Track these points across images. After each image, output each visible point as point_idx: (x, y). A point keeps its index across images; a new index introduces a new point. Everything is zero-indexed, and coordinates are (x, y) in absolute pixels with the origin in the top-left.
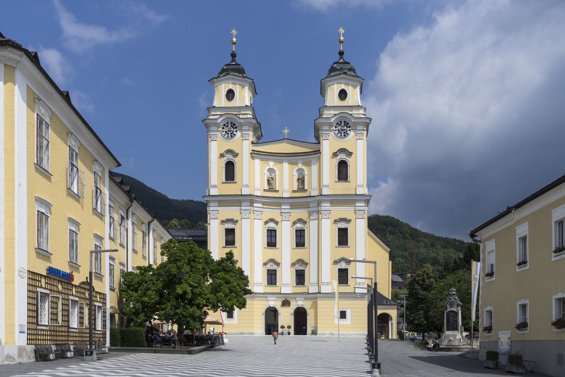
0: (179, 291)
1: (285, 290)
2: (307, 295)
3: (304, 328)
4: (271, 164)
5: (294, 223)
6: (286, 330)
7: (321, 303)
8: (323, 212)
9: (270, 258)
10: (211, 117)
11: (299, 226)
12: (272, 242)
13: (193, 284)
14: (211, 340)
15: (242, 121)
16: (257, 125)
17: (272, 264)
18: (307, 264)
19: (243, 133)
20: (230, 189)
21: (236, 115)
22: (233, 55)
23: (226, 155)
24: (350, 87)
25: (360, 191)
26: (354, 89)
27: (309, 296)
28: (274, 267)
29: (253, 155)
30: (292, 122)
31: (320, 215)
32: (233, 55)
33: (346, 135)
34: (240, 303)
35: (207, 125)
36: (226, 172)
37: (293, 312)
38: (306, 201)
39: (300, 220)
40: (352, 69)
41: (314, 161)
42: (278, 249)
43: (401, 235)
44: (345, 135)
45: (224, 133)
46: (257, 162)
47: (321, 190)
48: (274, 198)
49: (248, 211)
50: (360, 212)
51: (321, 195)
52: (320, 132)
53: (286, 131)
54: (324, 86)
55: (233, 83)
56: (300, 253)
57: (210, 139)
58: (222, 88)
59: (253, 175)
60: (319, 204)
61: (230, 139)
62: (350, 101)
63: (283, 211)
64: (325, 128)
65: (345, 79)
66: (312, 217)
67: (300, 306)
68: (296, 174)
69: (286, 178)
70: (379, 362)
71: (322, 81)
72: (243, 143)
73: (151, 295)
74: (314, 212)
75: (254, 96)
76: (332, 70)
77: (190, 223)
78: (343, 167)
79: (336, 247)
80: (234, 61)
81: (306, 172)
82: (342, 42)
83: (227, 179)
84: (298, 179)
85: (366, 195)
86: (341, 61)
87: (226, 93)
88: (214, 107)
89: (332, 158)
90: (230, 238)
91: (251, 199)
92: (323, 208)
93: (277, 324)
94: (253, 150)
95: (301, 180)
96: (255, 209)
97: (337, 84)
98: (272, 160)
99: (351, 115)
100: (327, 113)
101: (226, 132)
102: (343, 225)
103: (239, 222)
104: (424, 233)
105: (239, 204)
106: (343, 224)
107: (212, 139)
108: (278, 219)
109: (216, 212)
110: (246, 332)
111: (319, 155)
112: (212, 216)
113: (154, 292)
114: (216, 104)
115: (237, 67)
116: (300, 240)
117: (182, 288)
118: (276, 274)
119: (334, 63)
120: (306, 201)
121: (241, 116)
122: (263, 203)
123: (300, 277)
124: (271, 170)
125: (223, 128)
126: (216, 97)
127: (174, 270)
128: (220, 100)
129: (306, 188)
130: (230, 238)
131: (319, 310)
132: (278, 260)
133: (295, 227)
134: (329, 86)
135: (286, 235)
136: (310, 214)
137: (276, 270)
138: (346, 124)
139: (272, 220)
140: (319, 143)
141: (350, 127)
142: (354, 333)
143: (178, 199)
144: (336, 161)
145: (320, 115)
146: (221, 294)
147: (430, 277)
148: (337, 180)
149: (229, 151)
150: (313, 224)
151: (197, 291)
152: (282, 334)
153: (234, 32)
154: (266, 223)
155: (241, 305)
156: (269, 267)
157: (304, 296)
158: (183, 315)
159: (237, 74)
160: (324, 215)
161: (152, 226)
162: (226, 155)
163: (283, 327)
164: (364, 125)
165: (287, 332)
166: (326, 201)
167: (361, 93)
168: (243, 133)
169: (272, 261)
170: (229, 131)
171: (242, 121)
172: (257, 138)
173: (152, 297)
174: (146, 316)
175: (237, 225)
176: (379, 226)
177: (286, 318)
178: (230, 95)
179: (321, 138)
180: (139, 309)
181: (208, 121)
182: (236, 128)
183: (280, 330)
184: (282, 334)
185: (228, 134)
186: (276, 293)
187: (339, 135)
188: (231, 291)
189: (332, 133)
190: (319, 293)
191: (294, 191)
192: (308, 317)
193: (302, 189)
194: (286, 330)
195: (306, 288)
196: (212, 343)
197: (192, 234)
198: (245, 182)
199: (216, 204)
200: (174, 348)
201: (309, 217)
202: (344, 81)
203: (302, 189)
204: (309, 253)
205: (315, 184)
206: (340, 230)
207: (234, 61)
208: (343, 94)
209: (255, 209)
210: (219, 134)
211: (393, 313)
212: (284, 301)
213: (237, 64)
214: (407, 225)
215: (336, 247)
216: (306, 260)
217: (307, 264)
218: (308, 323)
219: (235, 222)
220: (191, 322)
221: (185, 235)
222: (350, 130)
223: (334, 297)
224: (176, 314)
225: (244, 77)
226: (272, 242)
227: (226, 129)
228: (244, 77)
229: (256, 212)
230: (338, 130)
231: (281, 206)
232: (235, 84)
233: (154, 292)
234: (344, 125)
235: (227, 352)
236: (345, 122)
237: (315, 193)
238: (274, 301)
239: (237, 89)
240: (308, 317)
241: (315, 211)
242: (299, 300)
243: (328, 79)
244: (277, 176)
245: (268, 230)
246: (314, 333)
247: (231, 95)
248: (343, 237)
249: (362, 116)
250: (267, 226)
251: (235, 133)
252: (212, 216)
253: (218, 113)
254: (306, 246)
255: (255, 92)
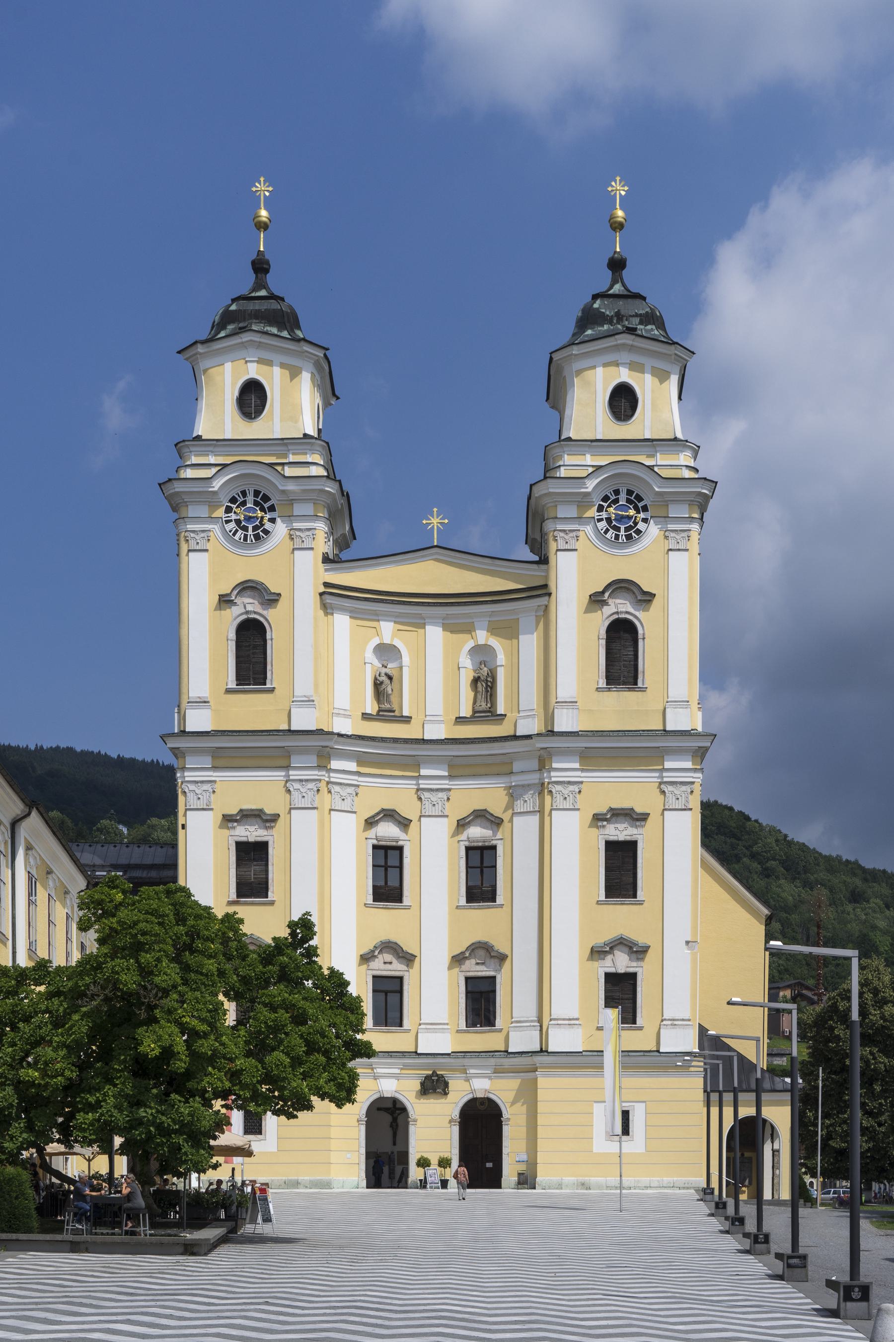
0: (150, 1047)
1: (430, 1043)
2: (502, 1059)
3: (489, 1165)
4: (388, 631)
5: (462, 825)
6: (434, 1173)
7: (549, 1086)
8: (555, 789)
9: (384, 937)
10: (189, 473)
11: (477, 833)
12: (388, 889)
13: (194, 1022)
14: (227, 1209)
15: (291, 487)
16: (341, 501)
17: (388, 957)
18: (502, 958)
19: (296, 525)
20: (252, 712)
21: (271, 465)
22: (260, 267)
23: (239, 600)
24: (648, 377)
25: (678, 720)
26: (662, 381)
27: (508, 1062)
28: (396, 968)
29: (329, 600)
30: (456, 490)
31: (548, 798)
32: (260, 267)
33: (633, 534)
34: (340, 1086)
35: (176, 501)
36: (238, 657)
37: (456, 1114)
38: (499, 751)
39: (481, 816)
40: (653, 318)
41: (526, 621)
42: (408, 908)
43: (755, 865)
44: (629, 537)
45: (232, 525)
46: (342, 622)
47: (549, 718)
48: (396, 740)
49: (310, 785)
50: (678, 790)
51: (551, 733)
52: (549, 526)
53: (435, 521)
54: (560, 370)
55: (260, 361)
56: (482, 923)
57: (184, 547)
58: (226, 377)
59: (328, 667)
60: (543, 763)
61: (252, 546)
62: (647, 423)
63: (424, 784)
64: (563, 511)
65: (631, 349)
66: (519, 806)
67: (480, 1095)
68: (467, 662)
69: (436, 675)
70: (863, 1279)
71: (556, 357)
72: (295, 559)
73: (53, 1061)
74: (526, 787)
75: (327, 404)
76: (588, 318)
77: (69, 823)
78: (622, 639)
79: (598, 903)
80: (264, 286)
81: (501, 658)
82: (621, 226)
83: (241, 678)
84: (476, 681)
85: (699, 735)
86: (617, 288)
87: (236, 393)
88: (199, 438)
89: (587, 611)
90: (252, 872)
91: (321, 745)
92: (556, 776)
93: (404, 1157)
94: (326, 585)
95: (485, 684)
96: (335, 777)
97: (605, 365)
98: (387, 617)
99: (651, 468)
100: (573, 464)
101: (238, 522)
102: (620, 832)
103: (281, 822)
104: (828, 859)
105: (283, 763)
106: (621, 826)
107: (193, 546)
108: (408, 808)
109: (207, 787)
110: (304, 1178)
111: (543, 601)
112: (193, 802)
113: (62, 1053)
114: (204, 428)
115: (274, 305)
116: (481, 879)
117: (160, 1038)
118: (401, 992)
119: (595, 297)
120: (499, 751)
121: (288, 471)
122: (362, 759)
123: (481, 1004)
124: (386, 651)
125: (228, 510)
126: (204, 404)
127: (130, 980)
128: (217, 416)
129: (500, 710)
130: (252, 872)
131: (541, 1107)
132: (409, 946)
133: (463, 837)
134: (579, 372)
135: (435, 865)
136: (513, 794)
137: (401, 979)
138: (635, 500)
139: (389, 815)
140: (544, 561)
141: (645, 509)
142: (655, 1180)
143: (22, 744)
144: (600, 621)
145: (547, 469)
146: (283, 1057)
147: (885, 1002)
148: (602, 683)
149: (249, 587)
150: (524, 829)
151: (205, 1046)
152: (423, 1184)
153: (262, 188)
154: (370, 823)
155: (343, 1094)
156: (474, 968)
157: (492, 1061)
158: (160, 1127)
159: (274, 330)
160: (559, 799)
161: (23, 831)
162: (239, 600)
163: (423, 1163)
164: (691, 503)
165: (437, 1180)
166: (566, 753)
167: (680, 398)
168: (296, 525)
169: (390, 947)
170: (248, 519)
171: (291, 487)
172: (336, 542)
173: (55, 1064)
174: (30, 1128)
175: (274, 832)
176: (727, 837)
177: (433, 1133)
178: (252, 398)
179: (553, 546)
180: (11, 1106)
181: (178, 487)
182: (272, 509)
183: (415, 1173)
184: (423, 1184)
185: (245, 529)
186: (403, 1054)
187: (611, 534)
188: (312, 1048)
189: (589, 529)
190: (543, 1051)
191: (460, 720)
192: (507, 1131)
193: (486, 711)
194: (434, 1173)
195: (500, 1037)
196: (231, 1214)
197: (123, 861)
198: (302, 688)
199: (207, 762)
200: (133, 1233)
201: (510, 806)
202: (625, 357)
203: (486, 711)
204: (510, 922)
205: (530, 697)
206: (611, 846)
207: (264, 286)
208: (623, 401)
209: (335, 777)
210: (216, 528)
211: (779, 1115)
212: (428, 1078)
213: (272, 297)
214: (774, 831)
215: (598, 903)
216: (501, 946)
217: (502, 958)
218: (505, 1151)
219: (268, 820)
220: (186, 1148)
221: (98, 861)
222: (645, 520)
223: (600, 1066)
224: (138, 1123)
225: (299, 340)
226: (388, 889)
227: (239, 513)
228: (299, 340)
229: (337, 788)
230: (609, 520)
231: (417, 766)
232: (269, 363)
233: (62, 1053)
234: (628, 504)
235: (289, 1246)
236: (630, 493)
237: (530, 726)
238: (397, 1077)
239: (273, 379)
240: (505, 1129)
241: (528, 787)
242: (478, 1076)
243: (575, 350)
244: (405, 671)
245: (375, 847)
246: (526, 1180)
247: (624, 404)
248: (621, 871)
249: (687, 474)
250: (372, 833)
251: (268, 526)
252: (193, 802)
253: (212, 460)
254: (500, 899)
255: (330, 389)
